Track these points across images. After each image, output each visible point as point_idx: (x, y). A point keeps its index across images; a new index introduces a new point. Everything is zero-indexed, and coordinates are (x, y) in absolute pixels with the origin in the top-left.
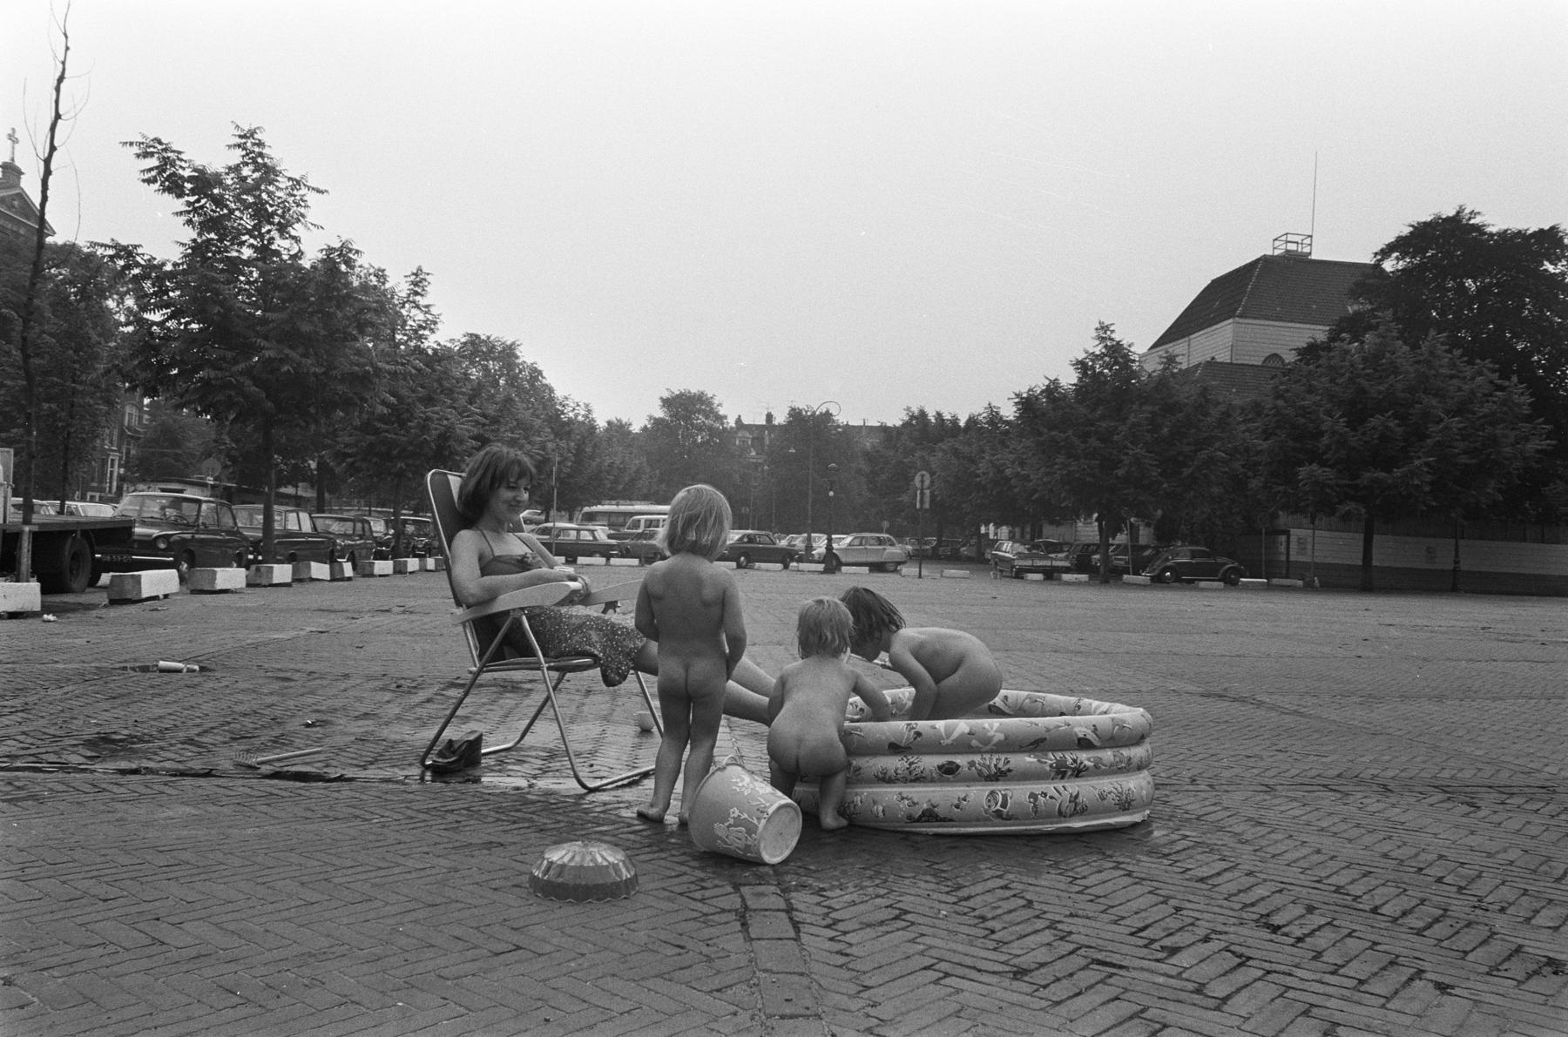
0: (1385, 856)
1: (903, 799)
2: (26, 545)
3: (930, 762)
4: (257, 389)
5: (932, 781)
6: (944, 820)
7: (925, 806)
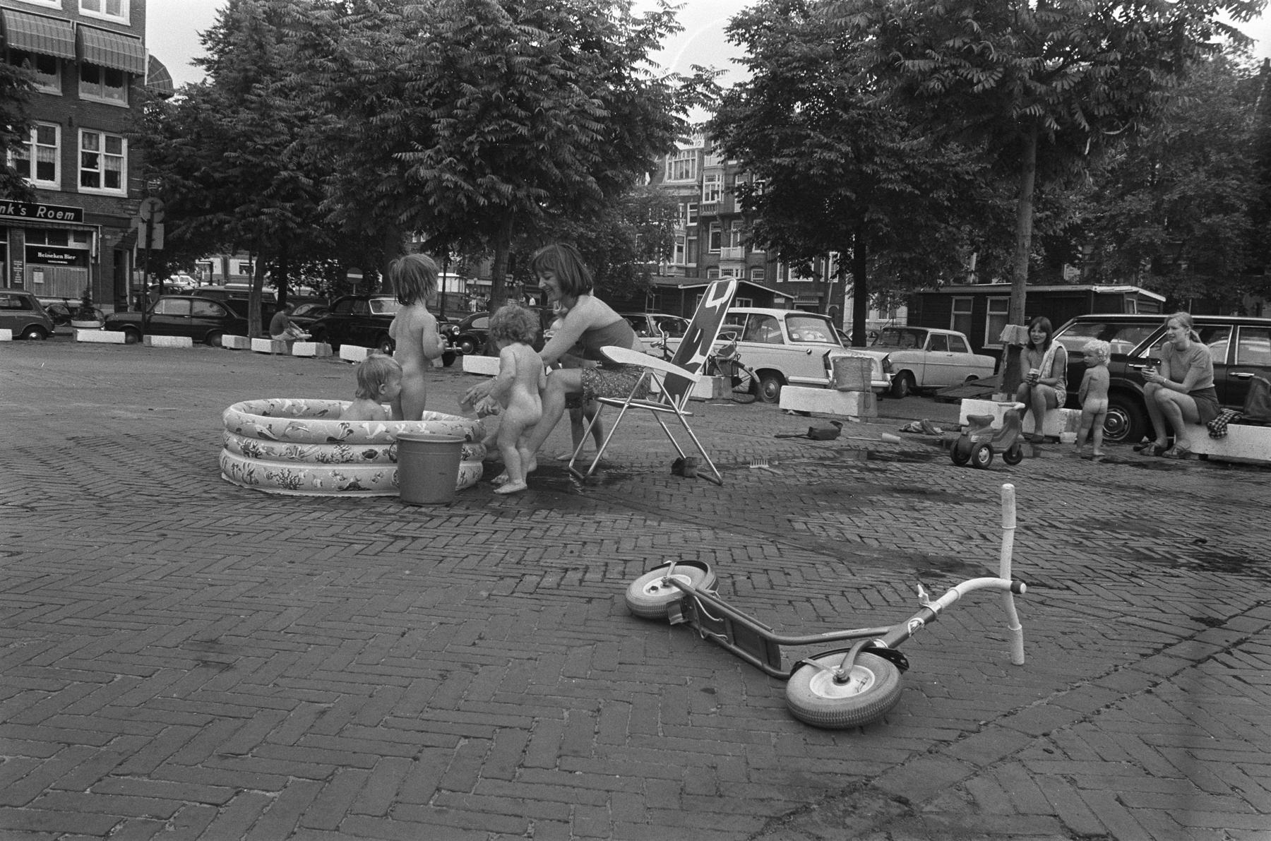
0: (414, 539)
1: (336, 475)
2: (952, 324)
3: (358, 450)
4: (597, 188)
5: (358, 462)
6: (364, 489)
7: (352, 480)
